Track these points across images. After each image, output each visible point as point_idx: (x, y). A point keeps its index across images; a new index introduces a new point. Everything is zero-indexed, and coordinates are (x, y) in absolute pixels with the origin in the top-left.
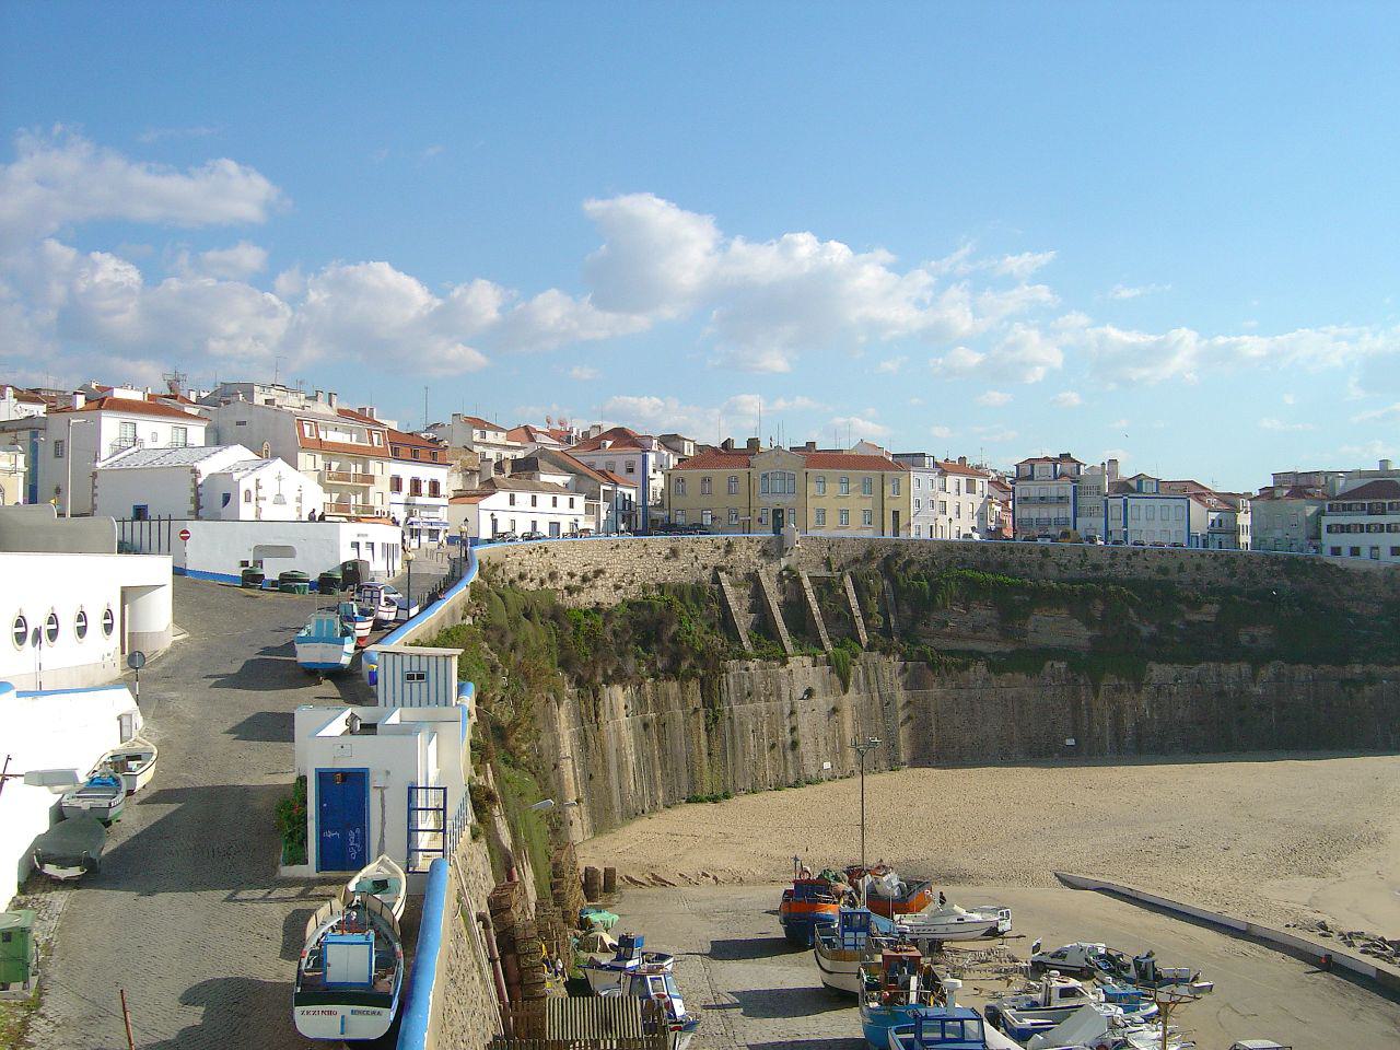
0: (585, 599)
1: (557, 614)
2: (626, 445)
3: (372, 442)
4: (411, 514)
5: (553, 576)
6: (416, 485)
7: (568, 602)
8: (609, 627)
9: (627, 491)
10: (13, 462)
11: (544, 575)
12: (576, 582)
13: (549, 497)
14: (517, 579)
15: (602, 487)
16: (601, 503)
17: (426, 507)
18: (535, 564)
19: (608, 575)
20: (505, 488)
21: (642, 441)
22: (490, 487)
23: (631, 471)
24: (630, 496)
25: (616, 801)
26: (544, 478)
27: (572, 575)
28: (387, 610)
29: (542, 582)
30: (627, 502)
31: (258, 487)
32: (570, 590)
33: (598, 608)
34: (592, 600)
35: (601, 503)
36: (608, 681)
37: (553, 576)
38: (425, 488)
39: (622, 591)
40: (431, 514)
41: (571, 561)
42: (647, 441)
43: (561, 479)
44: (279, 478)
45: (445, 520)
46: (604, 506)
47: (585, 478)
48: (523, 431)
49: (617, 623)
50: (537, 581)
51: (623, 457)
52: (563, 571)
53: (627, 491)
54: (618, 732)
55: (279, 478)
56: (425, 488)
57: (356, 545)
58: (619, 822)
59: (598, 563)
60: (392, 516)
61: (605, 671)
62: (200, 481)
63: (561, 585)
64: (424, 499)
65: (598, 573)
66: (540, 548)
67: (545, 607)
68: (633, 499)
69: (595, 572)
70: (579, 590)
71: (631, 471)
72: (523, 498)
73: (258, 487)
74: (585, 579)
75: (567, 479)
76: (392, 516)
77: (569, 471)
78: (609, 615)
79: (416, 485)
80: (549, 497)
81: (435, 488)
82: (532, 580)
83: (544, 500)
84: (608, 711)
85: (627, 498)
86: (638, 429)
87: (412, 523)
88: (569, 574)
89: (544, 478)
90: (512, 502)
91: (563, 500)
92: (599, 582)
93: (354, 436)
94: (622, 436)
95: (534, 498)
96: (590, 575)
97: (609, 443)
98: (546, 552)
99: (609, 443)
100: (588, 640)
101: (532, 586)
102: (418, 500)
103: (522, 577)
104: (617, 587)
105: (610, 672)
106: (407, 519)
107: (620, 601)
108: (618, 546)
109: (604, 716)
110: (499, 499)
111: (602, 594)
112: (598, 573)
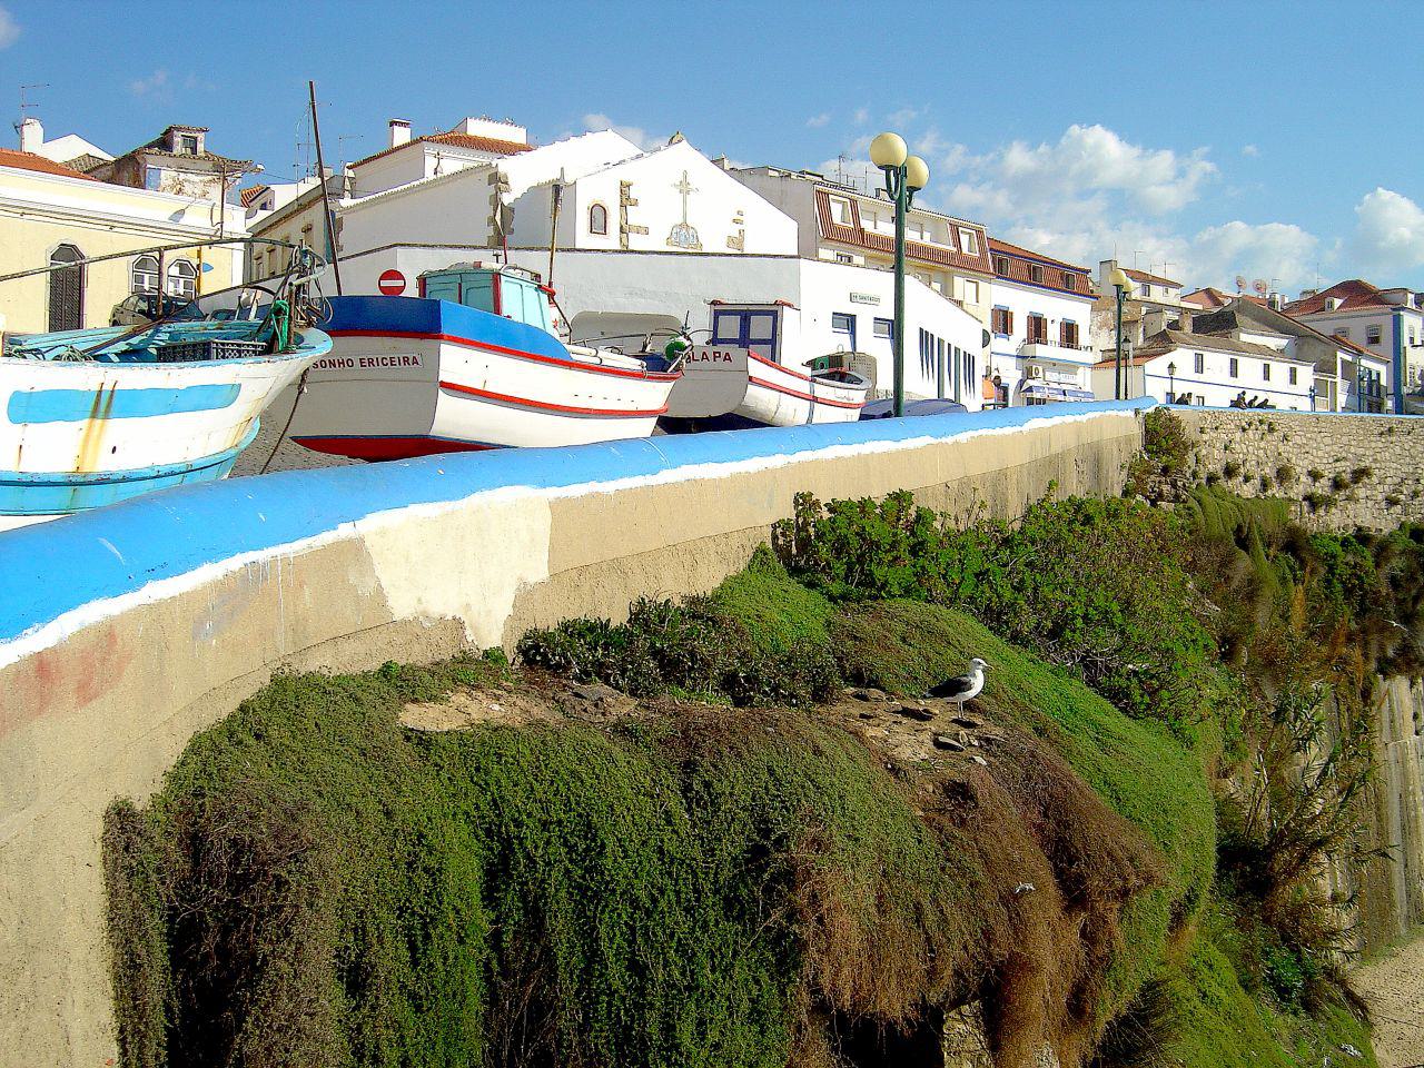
0: (1337, 520)
1: (1295, 544)
2: (1363, 303)
3: (958, 243)
4: (1028, 374)
5: (1283, 474)
6: (1037, 327)
7: (1312, 522)
8: (1386, 569)
9: (1375, 366)
10: (217, 219)
11: (1269, 471)
12: (1322, 488)
13: (1258, 364)
14: (1221, 474)
15: (1340, 355)
16: (1338, 379)
17: (1054, 364)
18: (1254, 452)
19: (1375, 479)
20: (1187, 344)
21: (1388, 297)
22: (1162, 342)
23: (1374, 340)
24: (1378, 375)
25: (1399, 894)
26: (1244, 337)
27: (1315, 476)
28: (804, 387)
29: (1265, 485)
30: (1374, 383)
31: (626, 201)
32: (1313, 502)
33: (1362, 537)
34: (1350, 522)
35: (1338, 379)
36: (1387, 668)
37: (1283, 474)
38: (1054, 332)
39: (1398, 509)
40: (1062, 378)
41: (1316, 455)
42: (1396, 297)
43: (1276, 342)
44: (684, 187)
45: (1087, 389)
46: (1342, 386)
47: (1311, 341)
48: (1205, 296)
49: (1397, 564)
50: (1257, 482)
51: (1358, 322)
52: (1301, 467)
53: (1375, 366)
54: (1402, 762)
55: (684, 187)
56: (1054, 332)
57: (848, 322)
58: (1403, 931)
59: (1359, 458)
60: (994, 374)
61: (1382, 648)
62: (507, 199)
63: (1298, 490)
64: (1051, 350)
65: (1360, 474)
66: (1261, 422)
67: (1271, 527)
68: (1383, 382)
69: (1354, 472)
70: (1328, 502)
71: (1374, 340)
72: (1217, 361)
73: (626, 201)
74: (1337, 485)
75: (1284, 342)
76: (994, 374)
77: (1283, 330)
78: (1382, 550)
79: (1037, 327)
80: (1258, 364)
81: (1070, 334)
82: (1247, 479)
83: (1245, 363)
84: (1386, 725)
85: (1374, 377)
86: (1378, 279)
87: (1030, 389)
88: (1310, 473)
89: (1244, 337)
90: (1199, 368)
91: (1280, 370)
92: (1361, 492)
93: (927, 236)
94: (1355, 292)
95: (1234, 363)
96: (1347, 477)
97: (1338, 302)
98: (1271, 430)
99: (1338, 302)
100: (1348, 592)
101: (1248, 491)
102: (1040, 350)
103: (1230, 472)
104: (1392, 502)
105: (1390, 653)
106: (1022, 383)
107: (1395, 527)
108: (1390, 430)
109: (1381, 736)
110: (1182, 357)
111: (1365, 512)
112: (1360, 474)
